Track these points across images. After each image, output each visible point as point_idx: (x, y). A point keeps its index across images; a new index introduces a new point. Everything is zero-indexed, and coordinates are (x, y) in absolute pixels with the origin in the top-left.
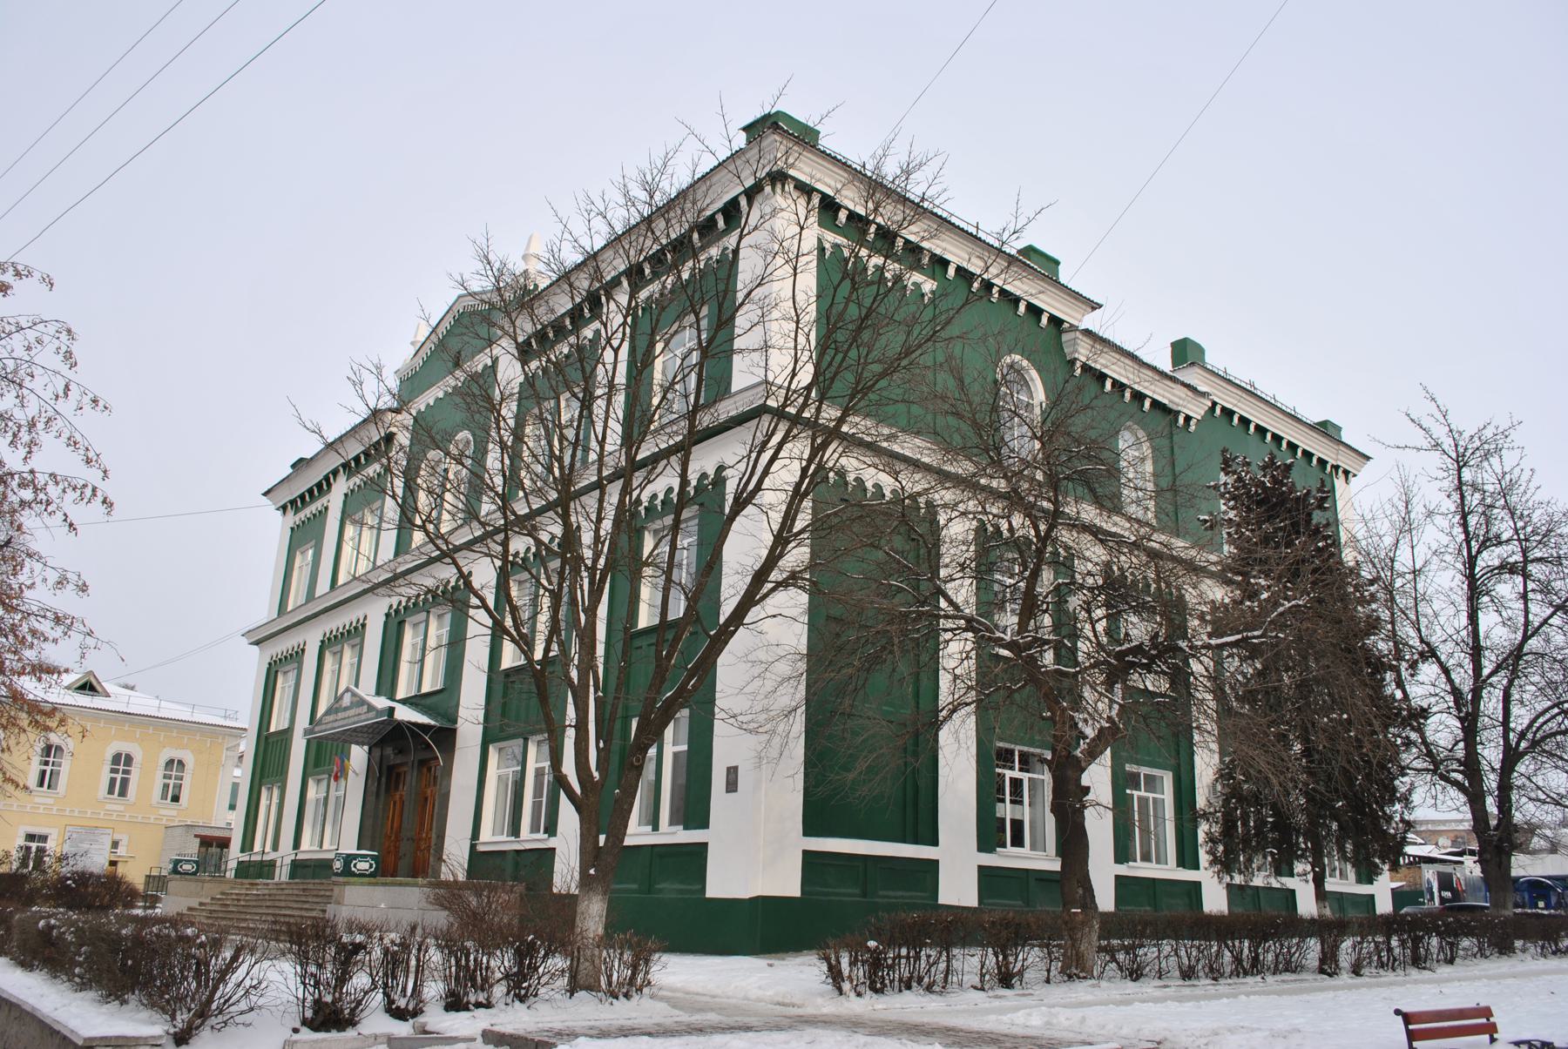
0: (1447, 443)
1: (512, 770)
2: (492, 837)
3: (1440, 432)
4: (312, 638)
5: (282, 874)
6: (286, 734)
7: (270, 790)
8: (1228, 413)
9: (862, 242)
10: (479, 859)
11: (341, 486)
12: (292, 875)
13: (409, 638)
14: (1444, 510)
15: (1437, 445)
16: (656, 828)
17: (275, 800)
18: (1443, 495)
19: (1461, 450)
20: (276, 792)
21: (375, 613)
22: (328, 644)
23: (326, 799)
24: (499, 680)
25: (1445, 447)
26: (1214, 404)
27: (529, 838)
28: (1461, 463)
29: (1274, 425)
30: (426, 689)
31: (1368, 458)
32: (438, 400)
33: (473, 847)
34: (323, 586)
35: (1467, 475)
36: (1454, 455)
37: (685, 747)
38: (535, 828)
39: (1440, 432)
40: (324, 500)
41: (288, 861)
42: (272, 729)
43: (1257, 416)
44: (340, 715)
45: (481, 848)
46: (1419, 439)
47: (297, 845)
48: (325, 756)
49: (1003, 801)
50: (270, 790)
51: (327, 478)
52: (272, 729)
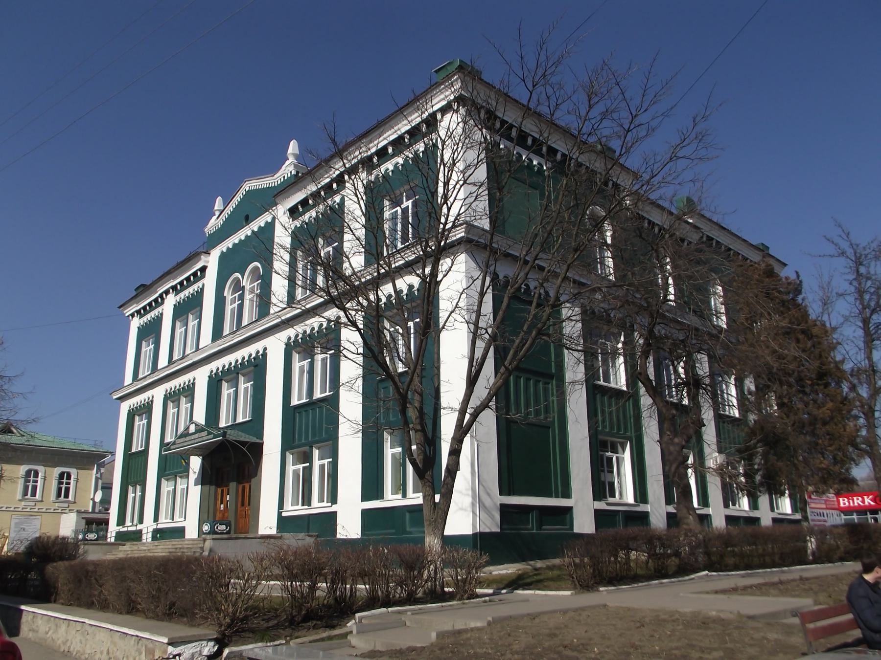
0: (850, 252)
1: (171, 488)
2: (293, 509)
3: (845, 245)
4: (158, 394)
5: (147, 537)
6: (145, 453)
7: (135, 487)
8: (710, 239)
9: (325, 200)
10: (284, 523)
11: (171, 301)
12: (154, 538)
13: (226, 391)
14: (849, 292)
15: (843, 253)
16: (404, 495)
17: (139, 493)
18: (847, 283)
19: (858, 255)
20: (138, 487)
21: (201, 377)
22: (171, 398)
23: (175, 491)
24: (290, 413)
25: (848, 254)
26: (703, 234)
27: (318, 506)
28: (858, 262)
29: (736, 246)
30: (240, 420)
31: (785, 265)
32: (235, 245)
33: (280, 514)
34: (163, 361)
35: (862, 270)
36: (853, 259)
37: (399, 450)
38: (321, 500)
39: (845, 245)
40: (160, 309)
41: (151, 530)
42: (134, 450)
43: (725, 240)
44: (188, 438)
45: (284, 514)
46: (831, 249)
47: (156, 519)
48: (172, 466)
49: (603, 471)
50: (135, 487)
51: (161, 296)
52: (134, 450)
